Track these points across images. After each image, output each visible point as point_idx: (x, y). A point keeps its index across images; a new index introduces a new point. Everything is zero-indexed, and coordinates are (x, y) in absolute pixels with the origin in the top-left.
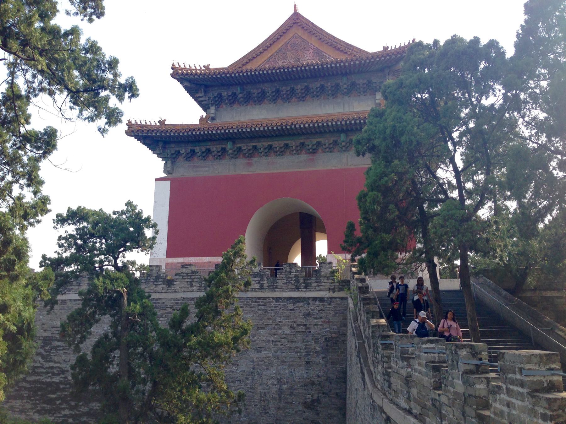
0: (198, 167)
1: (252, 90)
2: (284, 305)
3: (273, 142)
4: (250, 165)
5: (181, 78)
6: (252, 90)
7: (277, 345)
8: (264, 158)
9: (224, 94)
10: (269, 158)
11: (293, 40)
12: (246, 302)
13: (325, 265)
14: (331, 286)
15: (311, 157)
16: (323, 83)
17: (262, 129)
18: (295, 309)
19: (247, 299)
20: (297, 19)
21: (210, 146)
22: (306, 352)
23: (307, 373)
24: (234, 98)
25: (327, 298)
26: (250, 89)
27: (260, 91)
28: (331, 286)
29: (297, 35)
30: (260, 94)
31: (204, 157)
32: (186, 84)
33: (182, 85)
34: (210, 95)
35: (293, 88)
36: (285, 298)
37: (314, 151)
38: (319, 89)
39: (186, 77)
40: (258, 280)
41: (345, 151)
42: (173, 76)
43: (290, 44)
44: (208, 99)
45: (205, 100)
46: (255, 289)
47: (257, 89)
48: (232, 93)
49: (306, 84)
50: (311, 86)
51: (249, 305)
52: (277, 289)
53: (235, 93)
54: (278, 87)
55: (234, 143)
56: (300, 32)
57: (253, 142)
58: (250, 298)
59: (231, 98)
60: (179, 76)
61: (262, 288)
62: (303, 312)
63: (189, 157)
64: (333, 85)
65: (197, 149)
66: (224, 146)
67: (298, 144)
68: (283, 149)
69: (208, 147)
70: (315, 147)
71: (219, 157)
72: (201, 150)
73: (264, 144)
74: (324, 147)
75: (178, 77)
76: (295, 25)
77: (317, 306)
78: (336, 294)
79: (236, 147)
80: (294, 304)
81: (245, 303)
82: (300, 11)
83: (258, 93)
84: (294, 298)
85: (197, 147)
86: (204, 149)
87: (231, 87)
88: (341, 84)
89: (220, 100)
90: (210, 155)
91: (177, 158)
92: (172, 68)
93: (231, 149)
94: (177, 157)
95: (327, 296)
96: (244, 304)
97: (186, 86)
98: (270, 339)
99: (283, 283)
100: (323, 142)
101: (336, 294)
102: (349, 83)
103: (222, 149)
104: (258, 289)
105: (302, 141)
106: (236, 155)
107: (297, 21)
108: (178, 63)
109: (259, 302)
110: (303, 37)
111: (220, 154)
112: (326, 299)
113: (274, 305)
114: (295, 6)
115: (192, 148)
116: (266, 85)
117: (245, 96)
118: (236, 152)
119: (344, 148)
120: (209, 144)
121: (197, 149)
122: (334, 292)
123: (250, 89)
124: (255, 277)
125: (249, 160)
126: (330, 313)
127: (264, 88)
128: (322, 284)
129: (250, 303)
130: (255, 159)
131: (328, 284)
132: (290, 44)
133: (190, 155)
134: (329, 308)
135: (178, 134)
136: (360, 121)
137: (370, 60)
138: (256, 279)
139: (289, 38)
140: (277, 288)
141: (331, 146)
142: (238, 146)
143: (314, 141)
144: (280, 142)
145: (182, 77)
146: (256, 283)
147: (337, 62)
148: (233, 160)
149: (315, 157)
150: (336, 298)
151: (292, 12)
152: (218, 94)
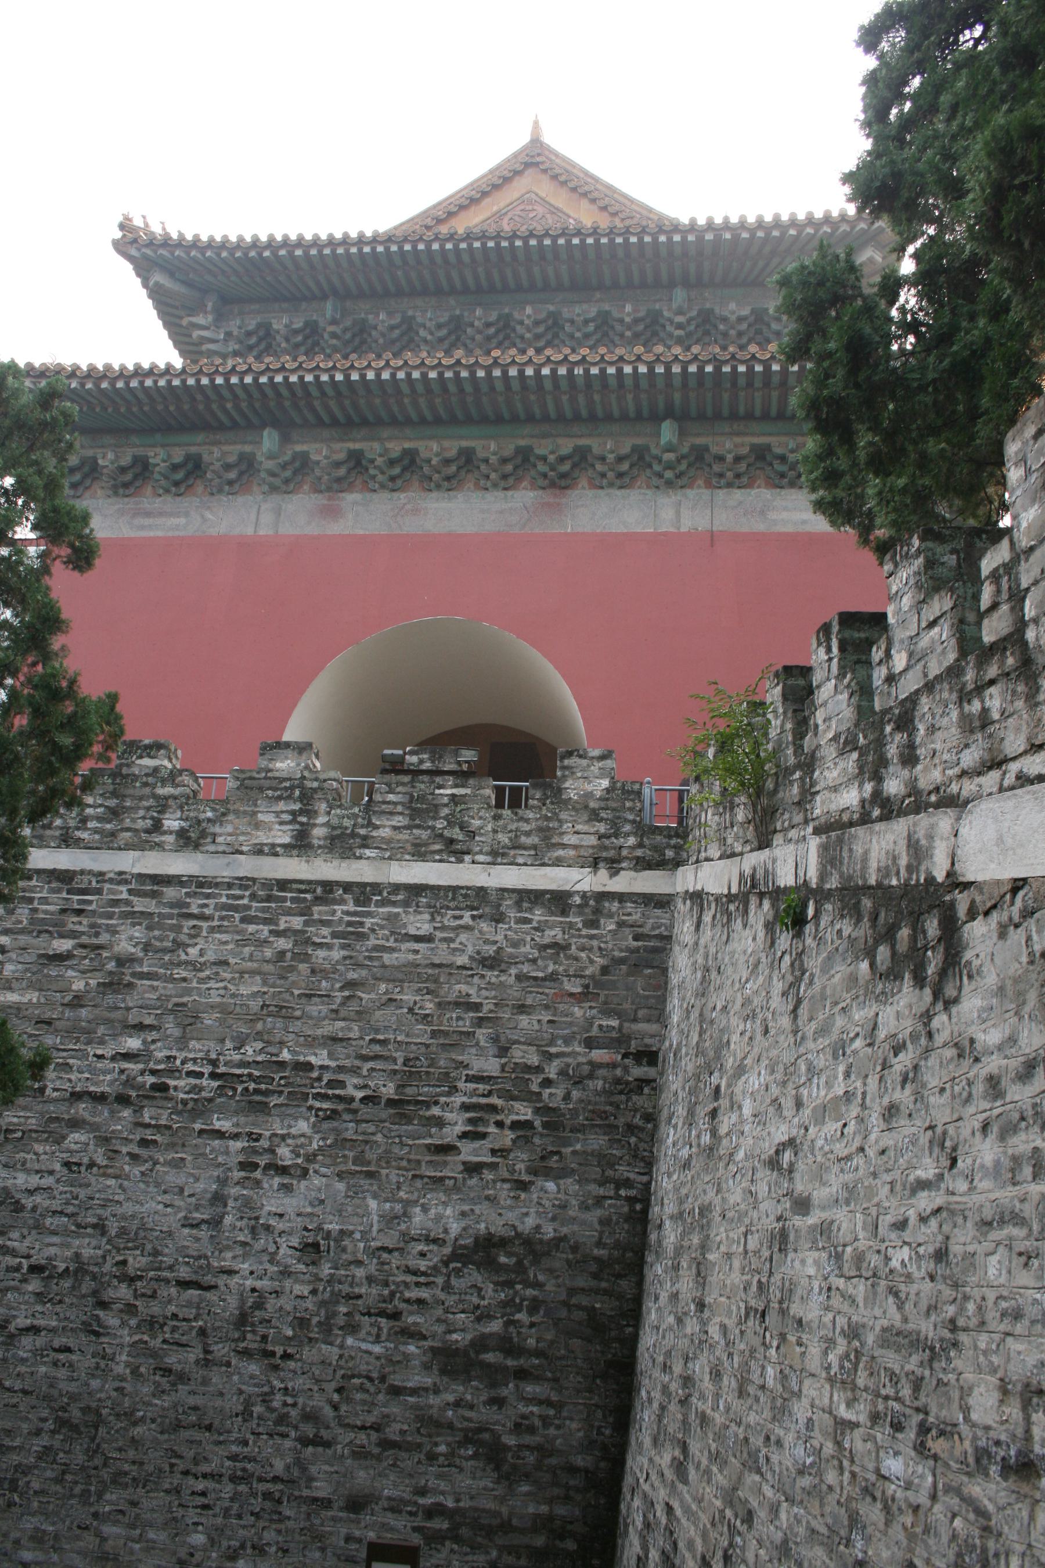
0: (148, 514)
1: (370, 317)
2: (392, 918)
3: (421, 443)
4: (332, 512)
5: (145, 257)
6: (370, 317)
7: (342, 1084)
8: (386, 495)
9: (279, 324)
10: (402, 496)
11: (522, 207)
12: (228, 896)
13: (584, 762)
14: (606, 848)
15: (551, 500)
16: (607, 308)
17: (386, 375)
18: (439, 935)
19: (230, 886)
20: (539, 155)
21: (197, 444)
22: (471, 1121)
23: (463, 1214)
24: (310, 341)
25: (584, 895)
26: (366, 313)
27: (397, 320)
28: (606, 848)
29: (533, 196)
30: (397, 332)
31: (177, 484)
32: (158, 277)
33: (145, 285)
34: (234, 326)
35: (509, 316)
36: (396, 888)
37: (563, 483)
38: (591, 327)
39: (161, 251)
40: (293, 813)
41: (669, 484)
42: (120, 247)
43: (509, 215)
44: (225, 340)
45: (217, 341)
46: (273, 846)
47: (390, 314)
48: (307, 324)
49: (551, 308)
50: (566, 313)
51: (236, 909)
52: (368, 852)
53: (316, 322)
54: (458, 312)
55: (286, 439)
56: (545, 188)
57: (350, 440)
58: (245, 882)
59: (300, 338)
60: (139, 250)
61: (301, 844)
62: (470, 949)
63: (126, 485)
64: (641, 314)
65: (158, 457)
66: (248, 448)
67: (509, 450)
68: (453, 468)
69: (193, 450)
70: (566, 467)
71: (227, 488)
72: (169, 456)
73: (389, 445)
74: (599, 467)
75: (134, 252)
76: (530, 171)
77: (536, 929)
78: (627, 882)
79: (289, 453)
80: (435, 913)
81: (224, 900)
82: (549, 138)
83: (392, 328)
84: (439, 888)
85: (158, 450)
86: (178, 456)
87: (304, 305)
88: (666, 314)
89: (262, 346)
90: (199, 482)
91: (87, 488)
92: (122, 227)
93: (271, 457)
94: (88, 482)
95: (584, 886)
96: (217, 907)
97: (157, 284)
98: (313, 1059)
99: (395, 828)
100: (596, 450)
101: (627, 882)
102: (694, 313)
103: (242, 457)
104: (284, 846)
105: (522, 443)
106: (287, 481)
107: (538, 159)
108: (144, 217)
109: (284, 899)
110: (552, 202)
111: (232, 475)
112: (577, 900)
113: (348, 913)
114: (536, 125)
115: (140, 451)
116: (419, 302)
117: (348, 336)
118: (288, 473)
119: (669, 474)
120: (200, 437)
121: (158, 457)
122: (614, 873)
123: (366, 313)
124: (280, 798)
125: (330, 499)
126: (591, 961)
127: (410, 313)
128: (566, 839)
129: (245, 901)
130: (351, 497)
131: (593, 840)
132: (509, 215)
133: (128, 477)
134: (592, 937)
135: (95, 384)
136: (734, 368)
137: (768, 233)
138: (282, 806)
139: (508, 201)
140: (365, 846)
141: (625, 466)
142: (299, 448)
143: (566, 446)
144: (446, 444)
145: (148, 252)
146: (281, 823)
147: (661, 230)
148: (276, 498)
149: (564, 501)
150: (621, 897)
151: (524, 139)
152: (259, 326)
